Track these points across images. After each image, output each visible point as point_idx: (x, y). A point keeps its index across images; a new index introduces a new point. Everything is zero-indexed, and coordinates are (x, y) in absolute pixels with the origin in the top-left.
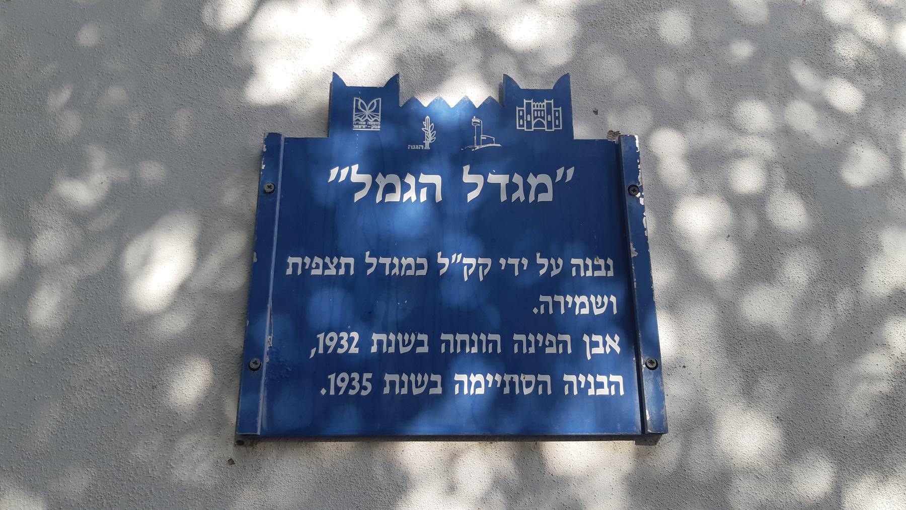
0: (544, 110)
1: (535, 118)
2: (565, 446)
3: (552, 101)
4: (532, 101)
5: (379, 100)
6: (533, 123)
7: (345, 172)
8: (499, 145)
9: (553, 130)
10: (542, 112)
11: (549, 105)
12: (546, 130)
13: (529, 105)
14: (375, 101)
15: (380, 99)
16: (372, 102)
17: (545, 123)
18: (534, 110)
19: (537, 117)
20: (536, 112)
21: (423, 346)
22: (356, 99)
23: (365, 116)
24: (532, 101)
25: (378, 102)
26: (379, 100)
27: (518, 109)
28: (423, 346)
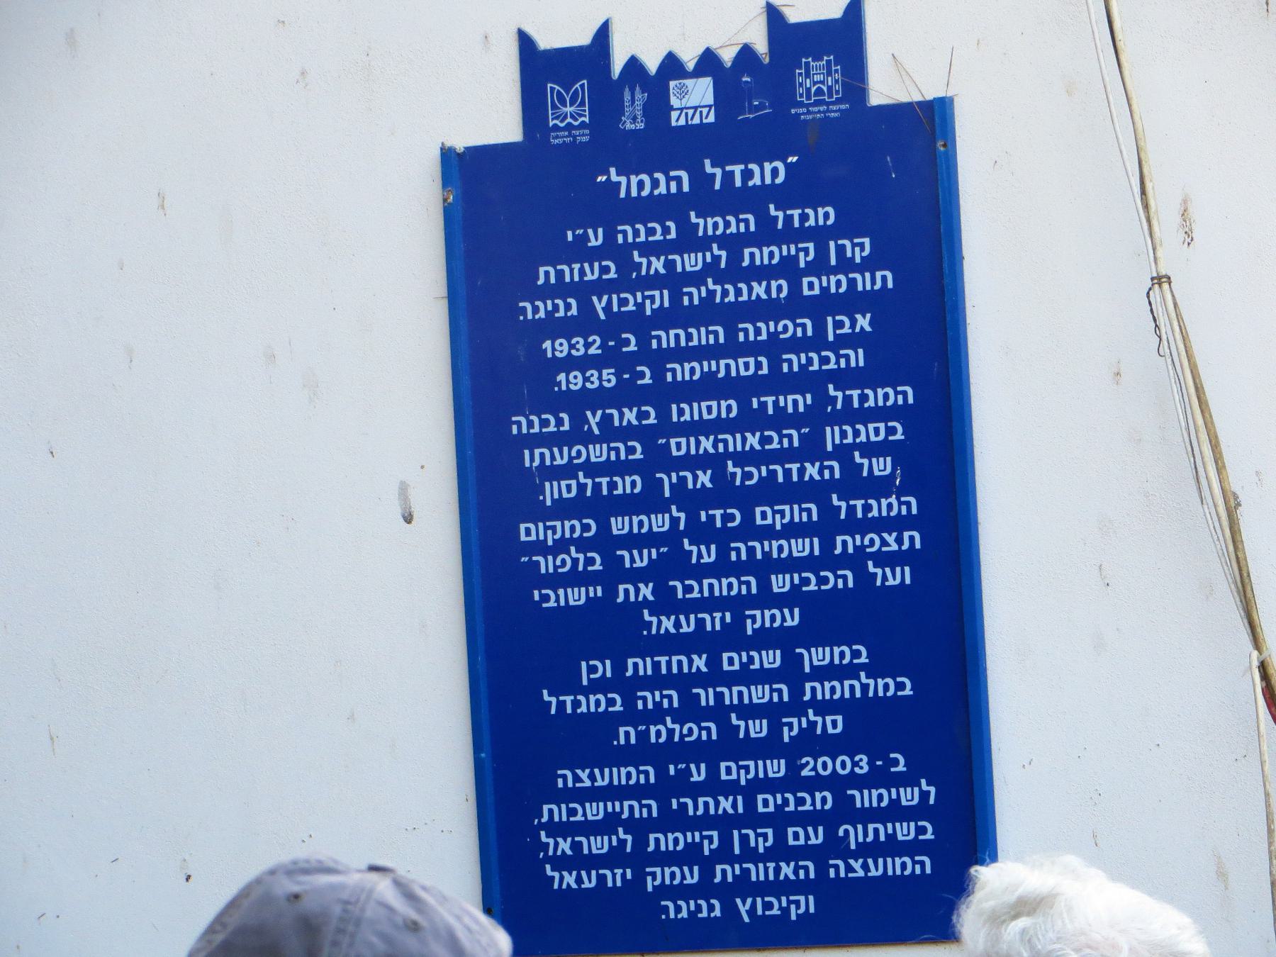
0: (823, 73)
1: (815, 83)
2: (1246, 660)
3: (832, 57)
4: (810, 59)
5: (584, 84)
6: (813, 90)
7: (785, 253)
8: (842, 847)
9: (834, 99)
10: (822, 76)
11: (829, 62)
12: (827, 100)
13: (807, 64)
14: (577, 85)
15: (585, 81)
16: (583, 82)
17: (825, 89)
18: (813, 74)
19: (818, 82)
20: (815, 76)
21: (764, 807)
22: (551, 87)
23: (565, 117)
24: (810, 59)
25: (582, 86)
26: (584, 84)
27: (797, 71)
28: (764, 807)
